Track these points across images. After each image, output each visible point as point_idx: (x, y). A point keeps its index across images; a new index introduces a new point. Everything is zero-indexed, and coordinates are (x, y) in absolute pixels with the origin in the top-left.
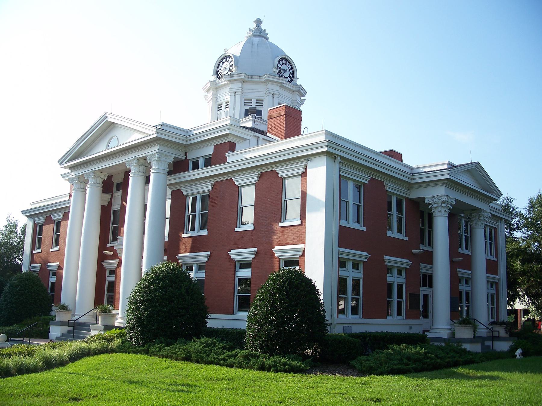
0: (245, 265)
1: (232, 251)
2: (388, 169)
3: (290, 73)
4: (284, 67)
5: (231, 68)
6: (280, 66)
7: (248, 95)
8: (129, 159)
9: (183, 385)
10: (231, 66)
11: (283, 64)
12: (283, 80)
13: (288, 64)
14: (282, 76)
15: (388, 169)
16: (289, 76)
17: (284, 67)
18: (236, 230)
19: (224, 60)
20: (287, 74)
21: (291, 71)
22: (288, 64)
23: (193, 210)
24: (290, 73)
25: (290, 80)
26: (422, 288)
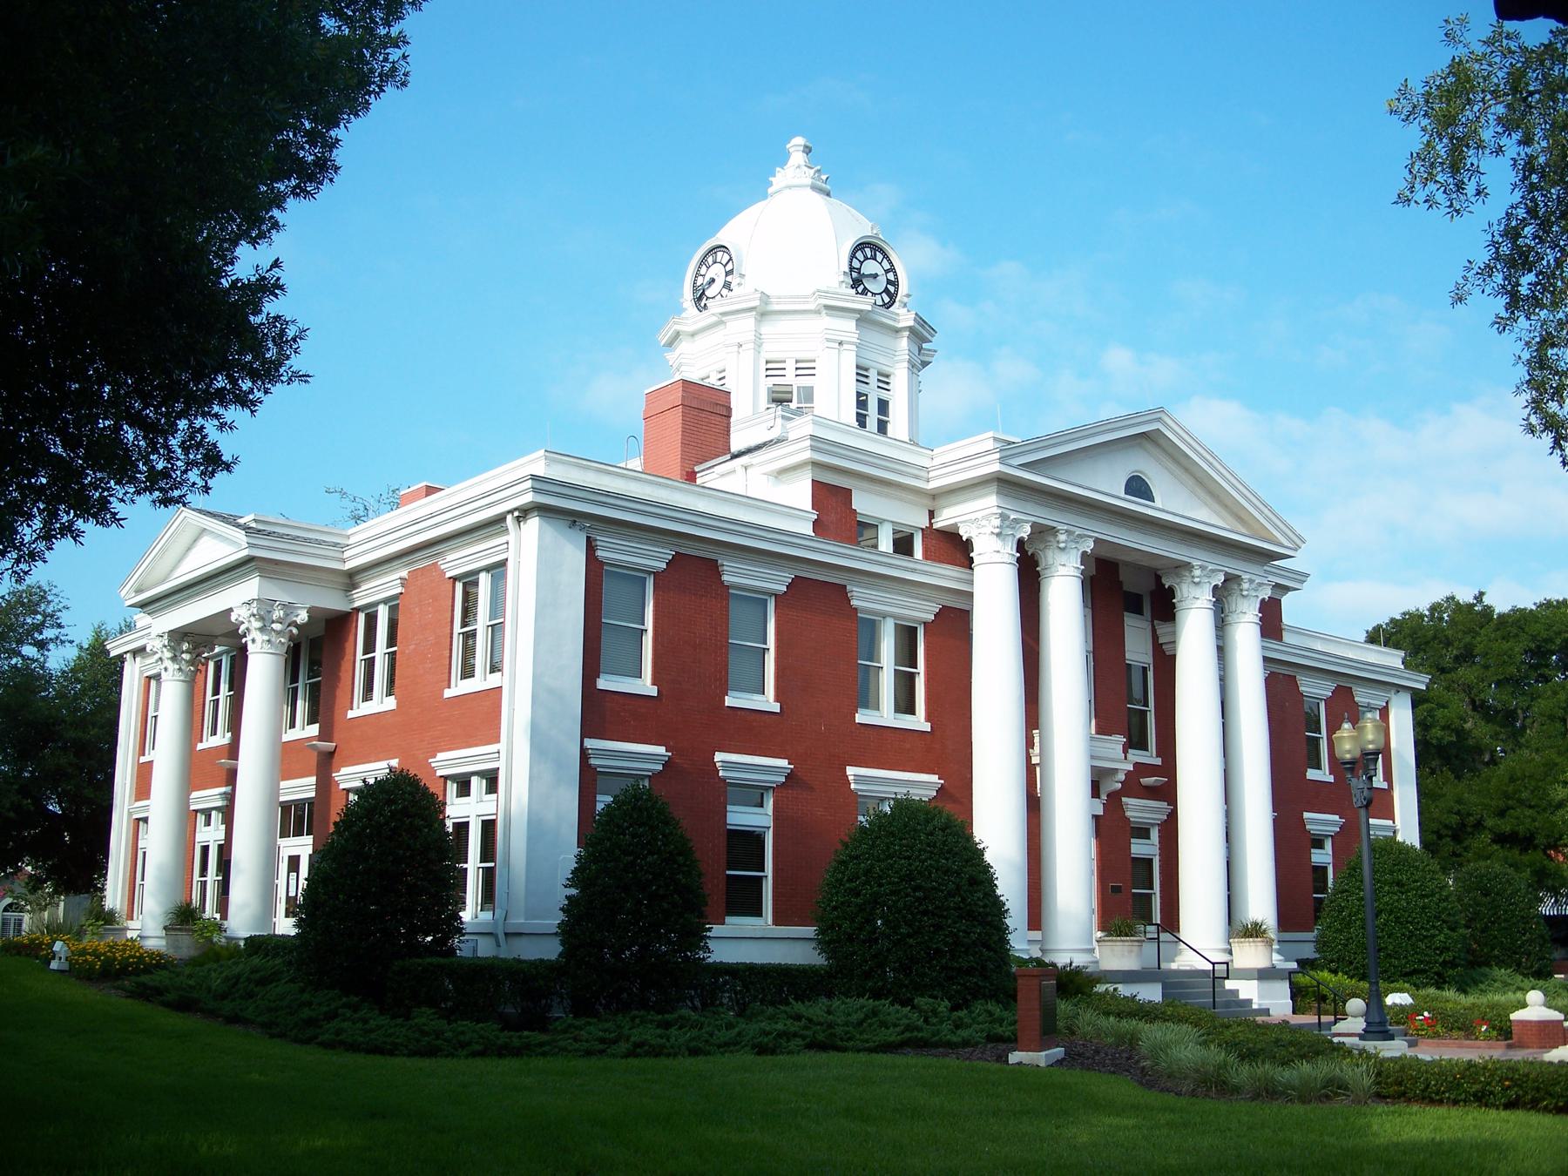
0: (753, 795)
1: (441, 756)
2: (489, 505)
3: (889, 282)
4: (870, 267)
5: (729, 279)
6: (856, 264)
7: (771, 351)
8: (1197, 557)
9: (1269, 1092)
10: (727, 274)
11: (866, 258)
12: (865, 303)
13: (879, 257)
14: (865, 291)
15: (489, 505)
16: (886, 291)
17: (870, 267)
18: (448, 693)
19: (710, 260)
20: (876, 286)
21: (891, 276)
22: (879, 257)
23: (370, 646)
24: (889, 282)
25: (887, 299)
26: (282, 842)
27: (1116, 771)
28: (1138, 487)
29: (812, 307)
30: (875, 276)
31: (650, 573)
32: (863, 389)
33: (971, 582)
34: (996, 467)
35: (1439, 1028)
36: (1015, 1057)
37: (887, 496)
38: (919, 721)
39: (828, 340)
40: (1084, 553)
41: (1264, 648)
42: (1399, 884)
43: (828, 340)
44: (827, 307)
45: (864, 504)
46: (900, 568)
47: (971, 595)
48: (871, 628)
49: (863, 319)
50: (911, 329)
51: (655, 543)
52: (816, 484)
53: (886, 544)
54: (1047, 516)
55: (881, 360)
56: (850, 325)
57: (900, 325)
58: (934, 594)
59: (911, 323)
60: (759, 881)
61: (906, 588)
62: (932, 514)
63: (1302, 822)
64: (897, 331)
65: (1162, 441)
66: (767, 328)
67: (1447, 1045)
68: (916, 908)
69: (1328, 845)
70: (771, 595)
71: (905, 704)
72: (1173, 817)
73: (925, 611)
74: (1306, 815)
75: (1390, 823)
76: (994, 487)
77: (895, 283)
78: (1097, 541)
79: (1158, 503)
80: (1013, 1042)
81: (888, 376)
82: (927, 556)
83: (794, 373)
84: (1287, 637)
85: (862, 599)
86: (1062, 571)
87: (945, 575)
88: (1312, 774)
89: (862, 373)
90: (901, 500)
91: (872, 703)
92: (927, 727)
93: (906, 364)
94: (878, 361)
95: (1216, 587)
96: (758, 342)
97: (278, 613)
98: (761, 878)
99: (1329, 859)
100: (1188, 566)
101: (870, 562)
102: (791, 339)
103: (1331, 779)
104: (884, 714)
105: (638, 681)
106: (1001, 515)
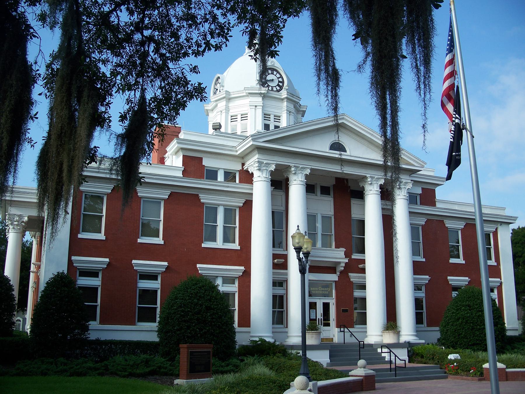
3: (279, 82)
7: (232, 112)
12: (264, 90)
13: (275, 73)
16: (278, 85)
21: (280, 80)
22: (275, 73)
24: (279, 82)
25: (278, 88)
27: (340, 263)
28: (337, 146)
29: (245, 94)
30: (273, 80)
31: (105, 194)
32: (267, 122)
33: (252, 189)
34: (251, 143)
35: (459, 371)
36: (177, 381)
37: (220, 159)
38: (236, 246)
39: (251, 106)
40: (306, 175)
41: (409, 208)
42: (469, 306)
43: (251, 106)
44: (250, 93)
45: (208, 162)
46: (231, 187)
47: (252, 194)
48: (214, 210)
49: (264, 96)
50: (287, 98)
51: (106, 183)
52: (184, 156)
53: (221, 177)
54: (284, 161)
55: (276, 111)
56: (260, 99)
57: (283, 97)
58: (242, 195)
59: (286, 96)
60: (155, 308)
61: (236, 195)
62: (243, 164)
63: (447, 281)
64: (283, 99)
65: (348, 127)
66: (231, 104)
67: (458, 379)
68: (203, 321)
69: (423, 288)
70: (162, 200)
71: (226, 240)
72: (501, 283)
73: (239, 202)
74: (449, 278)
75: (499, 280)
76: (256, 152)
77: (283, 82)
78: (312, 170)
79: (348, 153)
80: (178, 376)
81: (280, 117)
82: (240, 182)
83: (273, 120)
84: (438, 205)
85: (205, 199)
86: (295, 182)
87: (243, 188)
88: (452, 261)
89: (266, 116)
90: (228, 160)
91: (214, 239)
92: (239, 248)
93: (286, 112)
94: (273, 111)
95: (381, 185)
96: (227, 109)
97: (17, 218)
98: (156, 308)
99: (497, 297)
100: (365, 178)
101: (216, 185)
102: (239, 107)
103: (464, 262)
104: (219, 244)
105: (99, 234)
106: (258, 162)
